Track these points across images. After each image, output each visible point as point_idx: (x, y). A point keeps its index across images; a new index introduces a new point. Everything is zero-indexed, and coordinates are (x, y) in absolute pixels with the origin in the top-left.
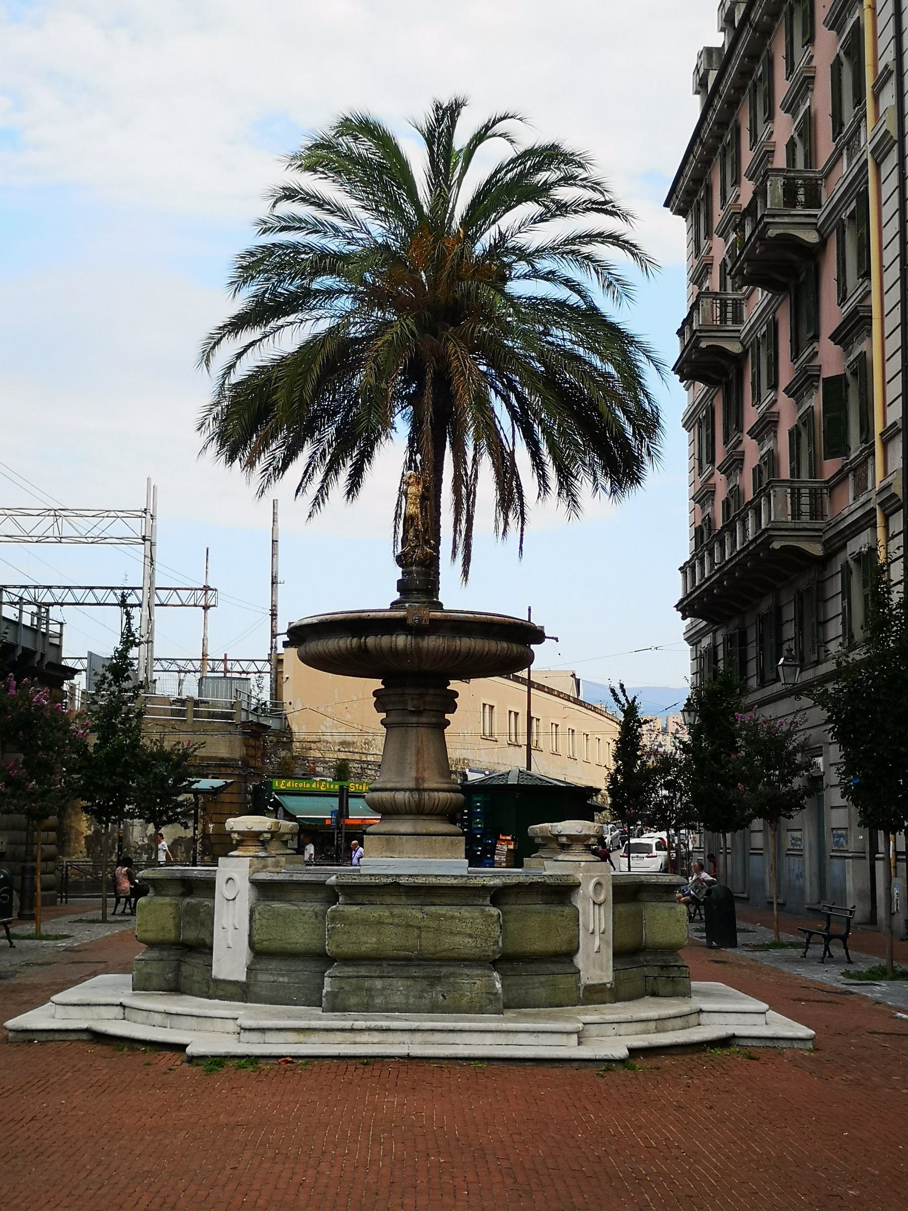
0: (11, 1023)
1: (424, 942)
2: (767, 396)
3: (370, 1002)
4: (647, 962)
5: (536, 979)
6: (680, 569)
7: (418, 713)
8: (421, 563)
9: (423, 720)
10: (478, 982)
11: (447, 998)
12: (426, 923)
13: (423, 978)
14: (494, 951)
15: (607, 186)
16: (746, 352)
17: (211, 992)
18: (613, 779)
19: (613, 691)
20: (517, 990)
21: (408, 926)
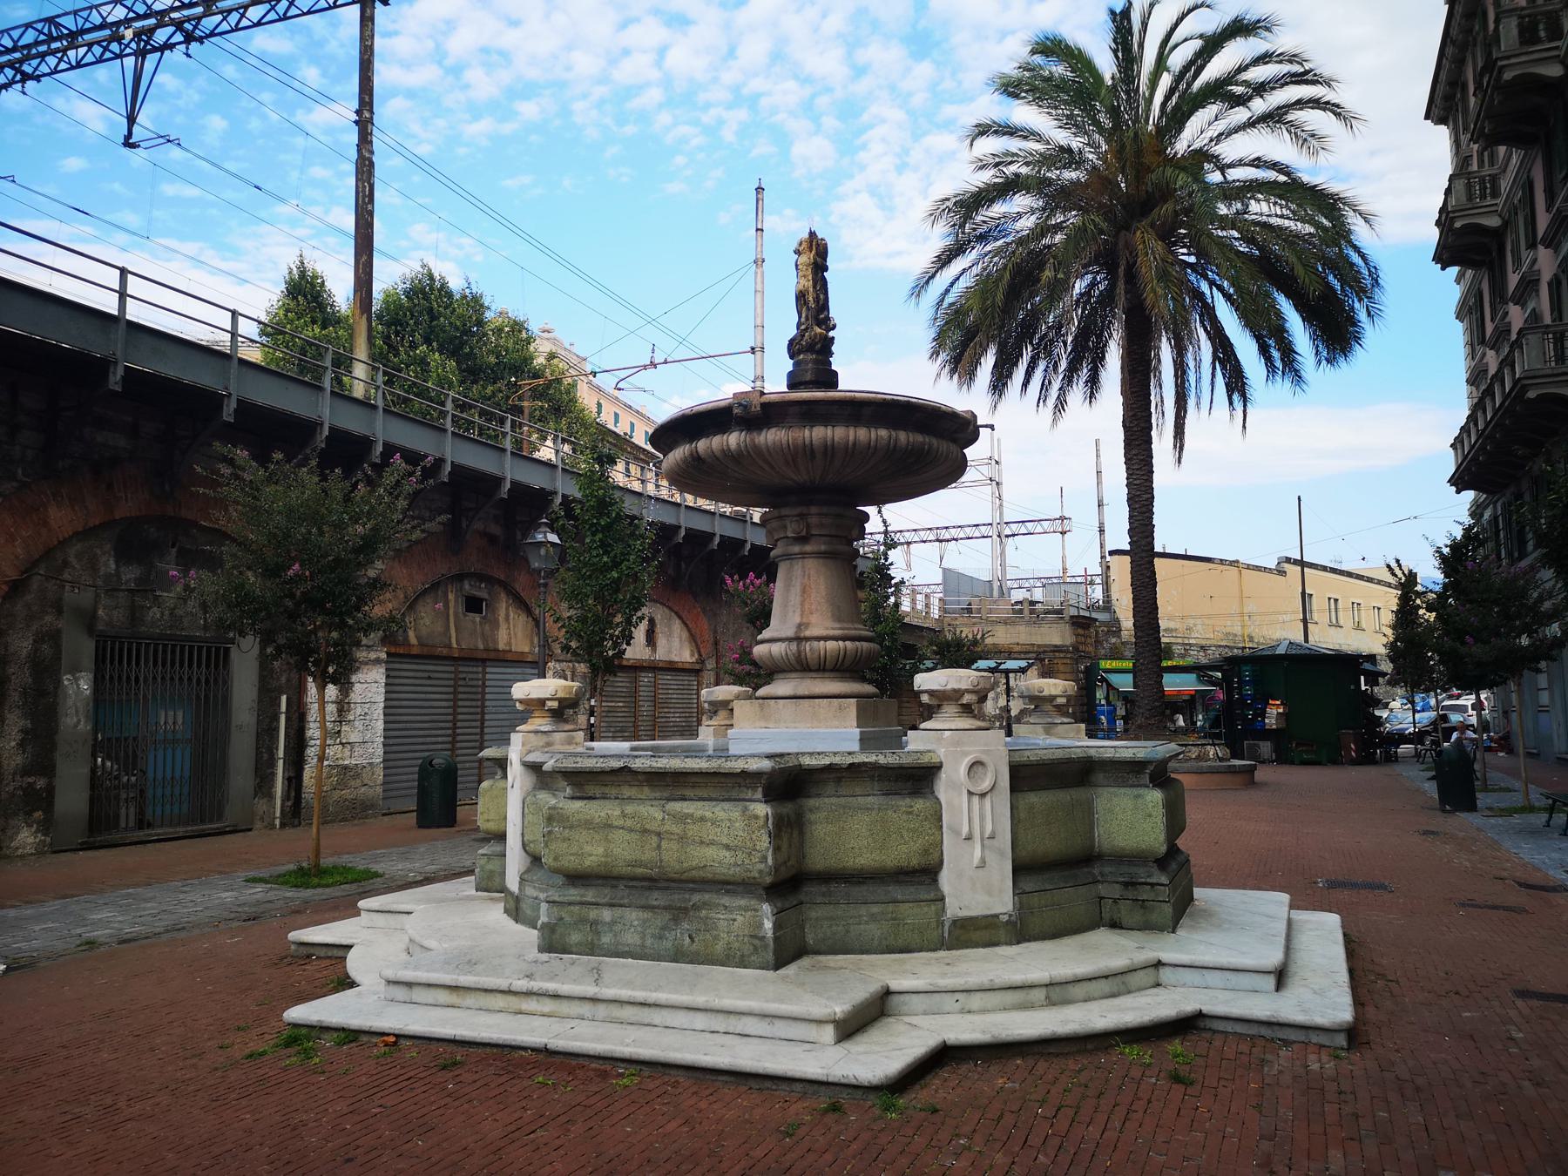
0: (295, 935)
1: (665, 857)
2: (1527, 256)
3: (596, 941)
4: (1103, 876)
5: (863, 910)
6: (1451, 446)
7: (802, 539)
8: (810, 348)
9: (808, 548)
10: (740, 918)
11: (696, 940)
12: (667, 827)
13: (665, 908)
14: (760, 872)
15: (1305, 56)
16: (1506, 224)
18: (1392, 646)
19: (1388, 566)
20: (831, 926)
21: (645, 831)
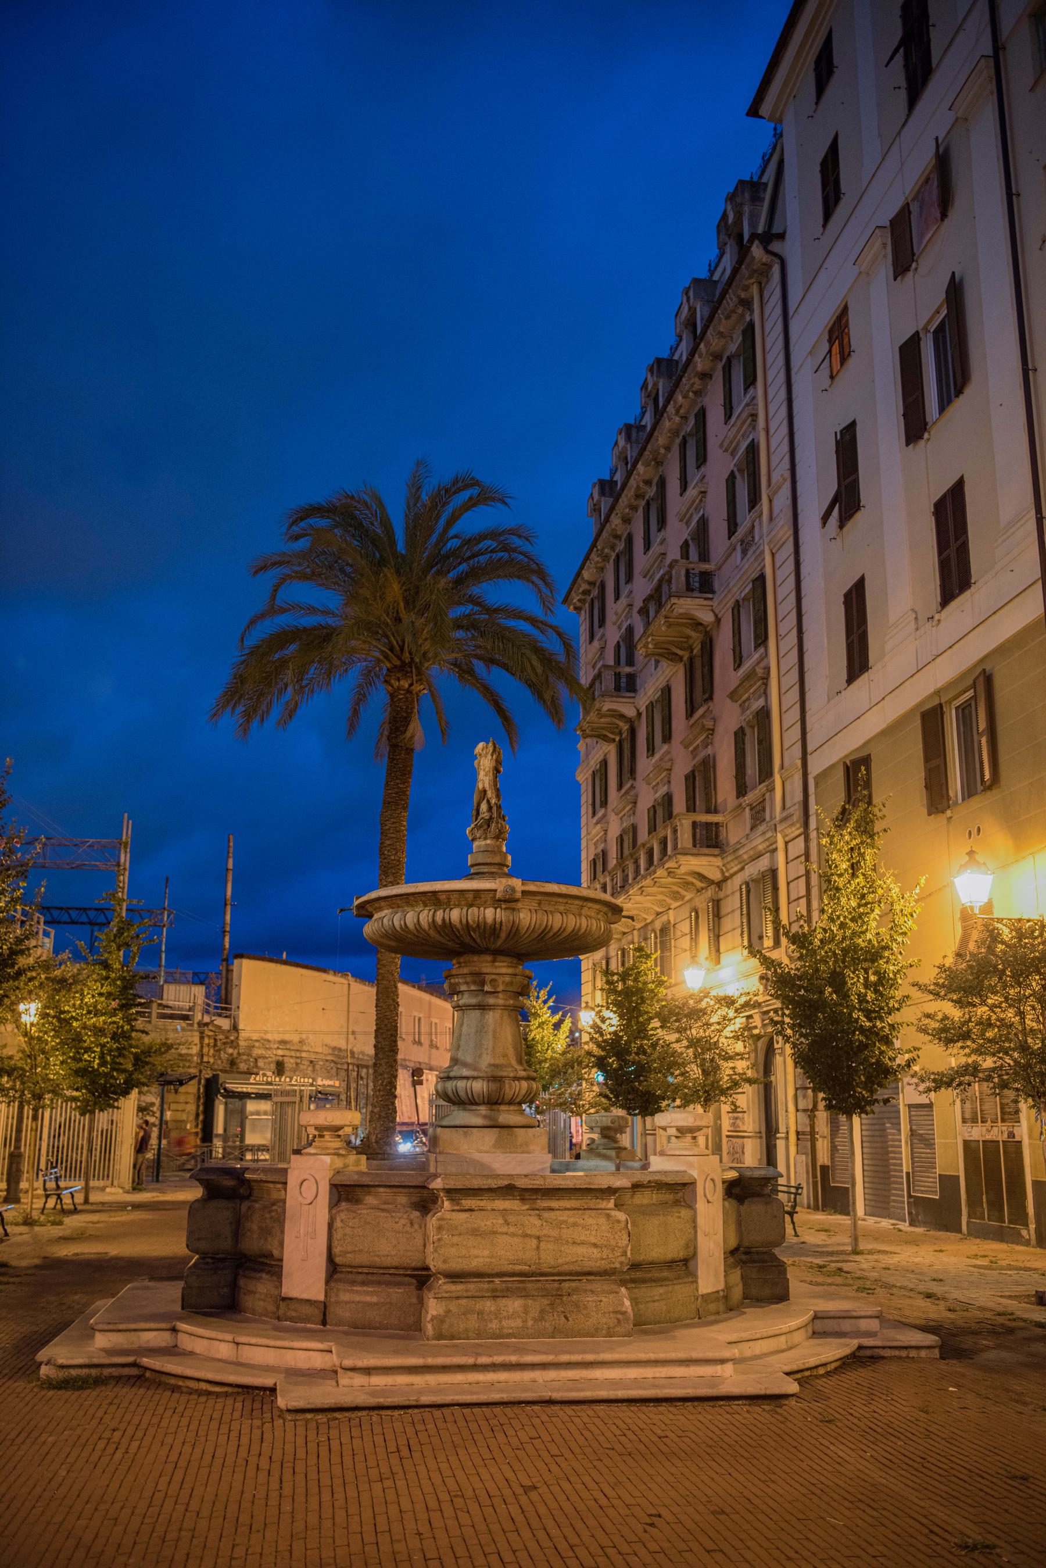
12: (545, 1232)
14: (621, 1263)
17: (281, 1312)
21: (526, 1236)
